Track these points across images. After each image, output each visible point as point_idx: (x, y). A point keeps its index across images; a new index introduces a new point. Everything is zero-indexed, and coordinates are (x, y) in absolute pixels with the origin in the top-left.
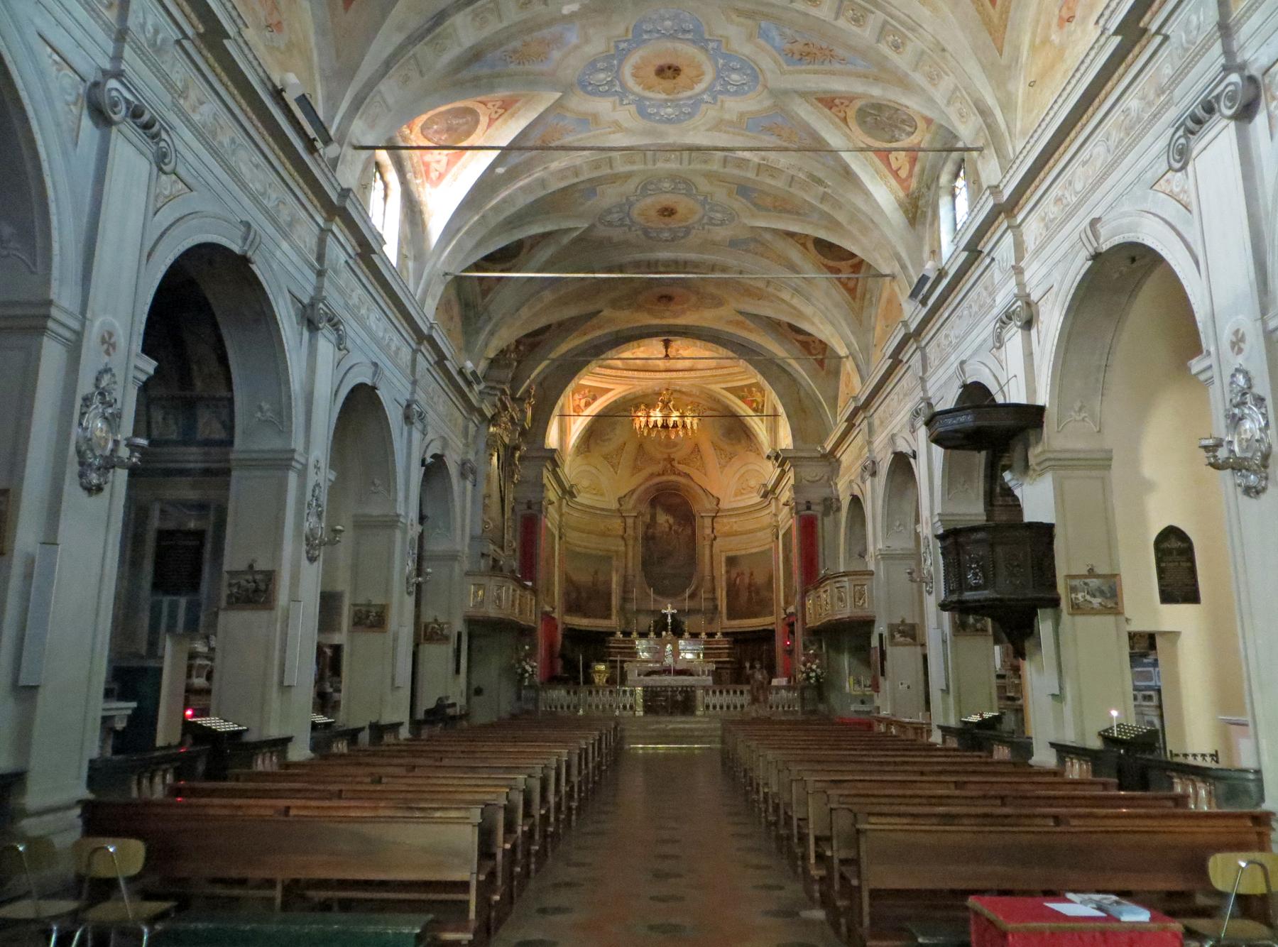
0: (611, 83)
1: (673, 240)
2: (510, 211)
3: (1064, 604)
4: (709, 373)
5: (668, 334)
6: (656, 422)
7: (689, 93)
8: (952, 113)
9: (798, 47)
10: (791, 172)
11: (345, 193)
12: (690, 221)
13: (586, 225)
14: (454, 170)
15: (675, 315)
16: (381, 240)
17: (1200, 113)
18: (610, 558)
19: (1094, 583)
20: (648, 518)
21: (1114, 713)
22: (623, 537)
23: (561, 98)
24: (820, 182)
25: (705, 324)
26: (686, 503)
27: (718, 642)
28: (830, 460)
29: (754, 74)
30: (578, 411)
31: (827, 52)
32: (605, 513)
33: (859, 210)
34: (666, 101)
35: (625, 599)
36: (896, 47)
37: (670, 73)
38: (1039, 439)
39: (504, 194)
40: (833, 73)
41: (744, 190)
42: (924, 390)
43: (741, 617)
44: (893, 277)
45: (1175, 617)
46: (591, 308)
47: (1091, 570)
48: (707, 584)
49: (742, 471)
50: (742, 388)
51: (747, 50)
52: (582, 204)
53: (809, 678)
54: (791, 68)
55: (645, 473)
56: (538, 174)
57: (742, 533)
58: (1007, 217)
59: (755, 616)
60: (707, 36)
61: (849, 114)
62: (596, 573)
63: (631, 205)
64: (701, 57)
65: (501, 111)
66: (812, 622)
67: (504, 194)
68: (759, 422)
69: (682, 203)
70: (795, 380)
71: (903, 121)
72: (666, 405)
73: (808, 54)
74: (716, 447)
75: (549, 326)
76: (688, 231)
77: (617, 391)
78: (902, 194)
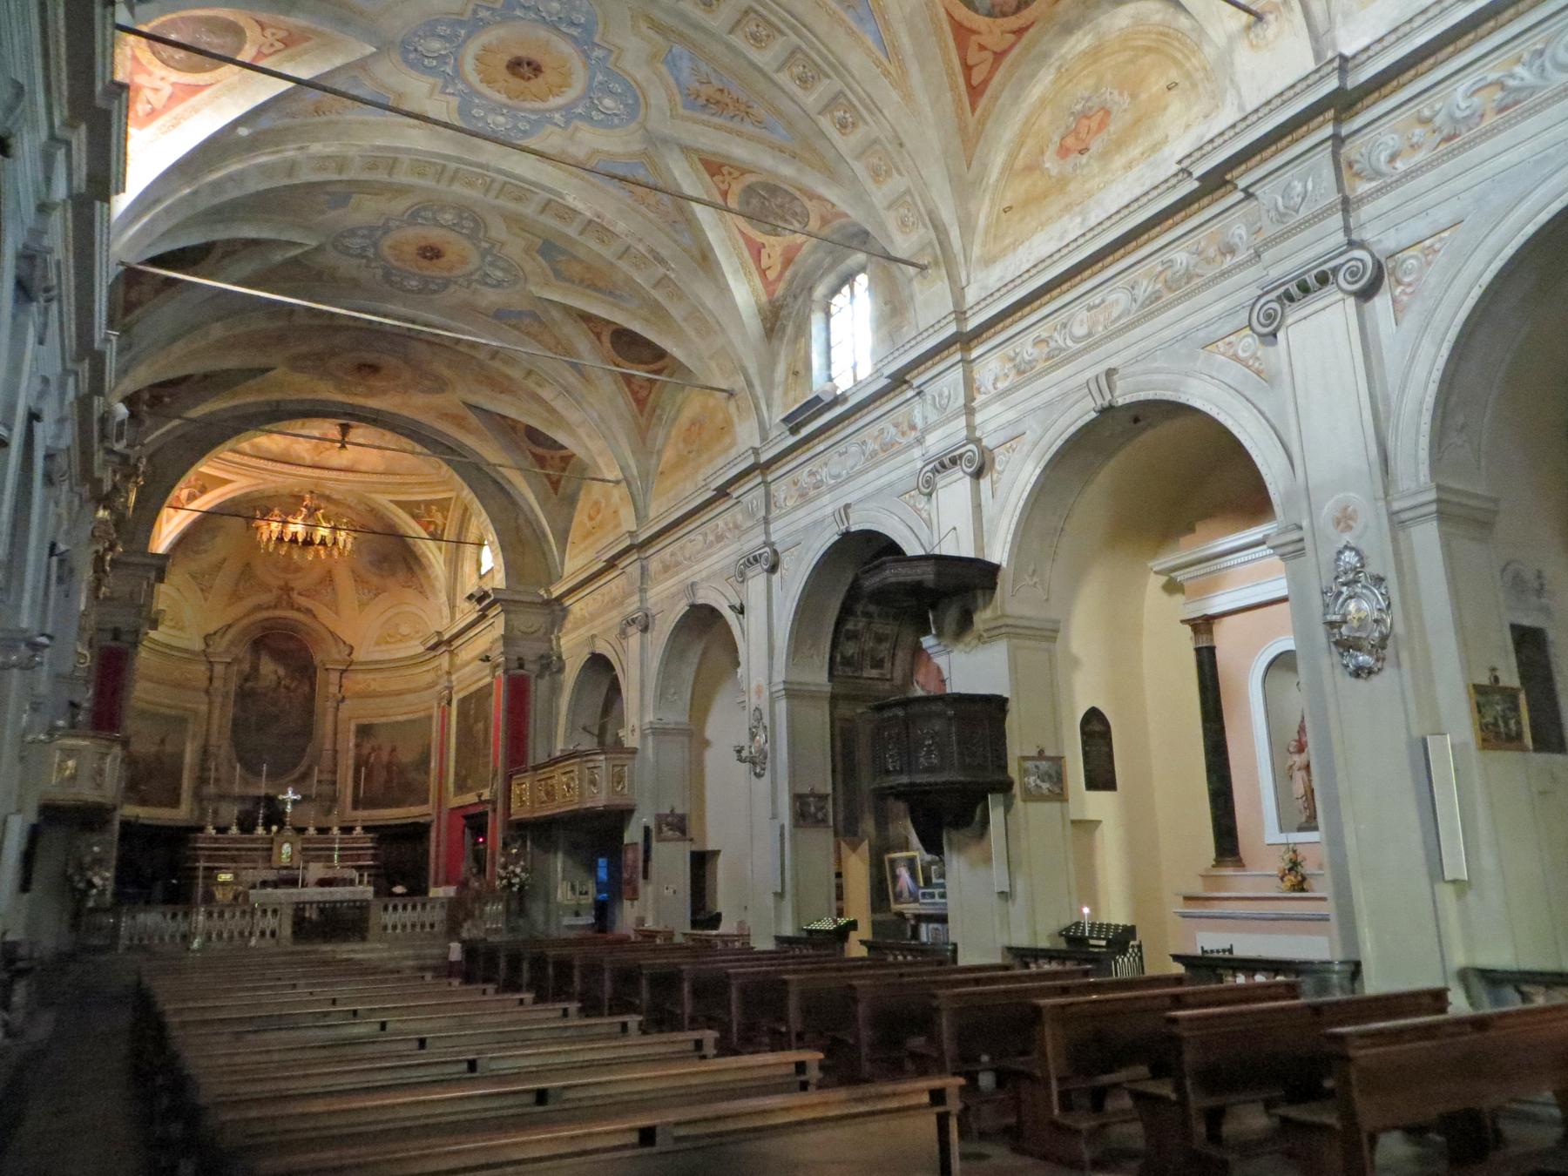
0: (442, 59)
1: (420, 291)
2: (233, 193)
3: (1017, 789)
4: (375, 478)
5: (349, 417)
6: (295, 534)
7: (538, 105)
8: (891, 220)
9: (706, 91)
10: (629, 241)
11: (121, 90)
12: (456, 272)
13: (314, 244)
14: (178, 110)
15: (371, 393)
16: (121, 188)
17: (1311, 279)
19: (1044, 765)
20: (246, 667)
21: (1086, 910)
22: (207, 692)
23: (373, 55)
24: (661, 261)
25: (405, 413)
26: (306, 649)
27: (355, 840)
28: (555, 610)
29: (634, 101)
31: (743, 108)
32: (189, 656)
33: (703, 305)
34: (506, 106)
35: (202, 780)
36: (843, 126)
37: (525, 69)
38: (988, 601)
39: (235, 167)
40: (740, 134)
41: (549, 249)
42: (767, 533)
44: (731, 394)
45: (1098, 805)
46: (259, 361)
47: (1041, 752)
48: (326, 761)
49: (389, 614)
50: (418, 504)
51: (641, 74)
52: (322, 212)
53: (511, 885)
54: (687, 113)
55: (249, 603)
56: (290, 152)
58: (962, 349)
59: (398, 803)
60: (597, 39)
61: (734, 186)
62: (163, 741)
63: (387, 230)
64: (577, 63)
65: (279, 45)
66: (519, 812)
67: (235, 167)
69: (456, 245)
70: (514, 503)
71: (795, 214)
72: (312, 512)
73: (718, 102)
74: (358, 579)
75: (190, 376)
76: (446, 283)
77: (238, 485)
78: (764, 299)
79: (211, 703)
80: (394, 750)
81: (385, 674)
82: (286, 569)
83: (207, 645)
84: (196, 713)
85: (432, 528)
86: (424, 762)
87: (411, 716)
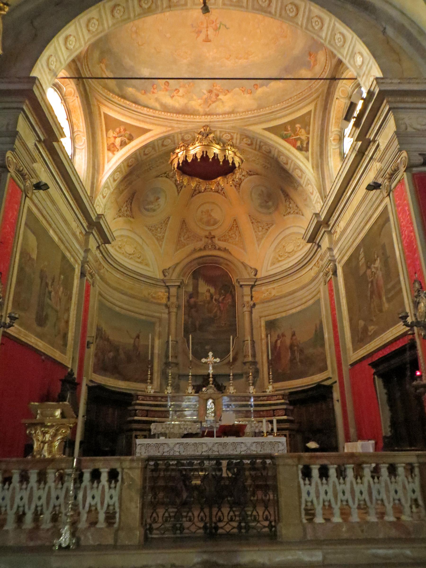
18: (153, 324)
20: (190, 289)
22: (167, 306)
26: (227, 275)
30: (112, 148)
32: (153, 282)
43: (284, 380)
50: (284, 126)
57: (281, 297)
62: (138, 337)
68: (305, 161)
74: (254, 220)
79: (169, 313)
80: (294, 334)
81: (280, 283)
82: (208, 223)
83: (165, 276)
84: (160, 319)
85: (299, 144)
86: (318, 338)
87: (303, 307)
